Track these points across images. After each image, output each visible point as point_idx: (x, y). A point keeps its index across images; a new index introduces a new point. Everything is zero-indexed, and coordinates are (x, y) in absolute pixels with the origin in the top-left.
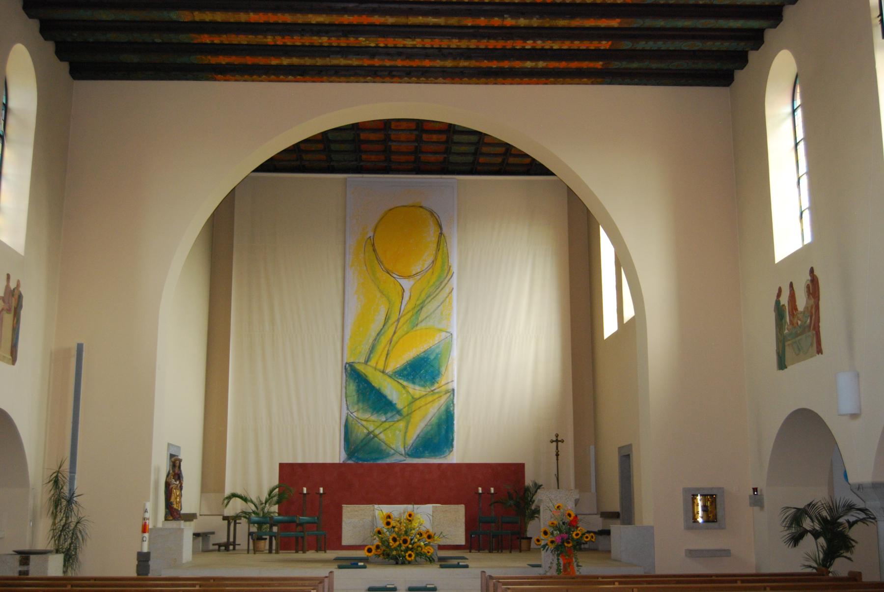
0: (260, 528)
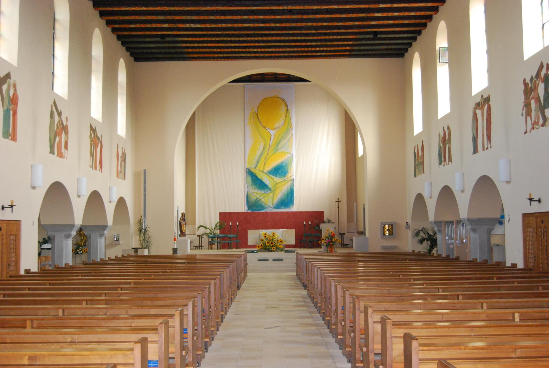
0: (212, 240)
